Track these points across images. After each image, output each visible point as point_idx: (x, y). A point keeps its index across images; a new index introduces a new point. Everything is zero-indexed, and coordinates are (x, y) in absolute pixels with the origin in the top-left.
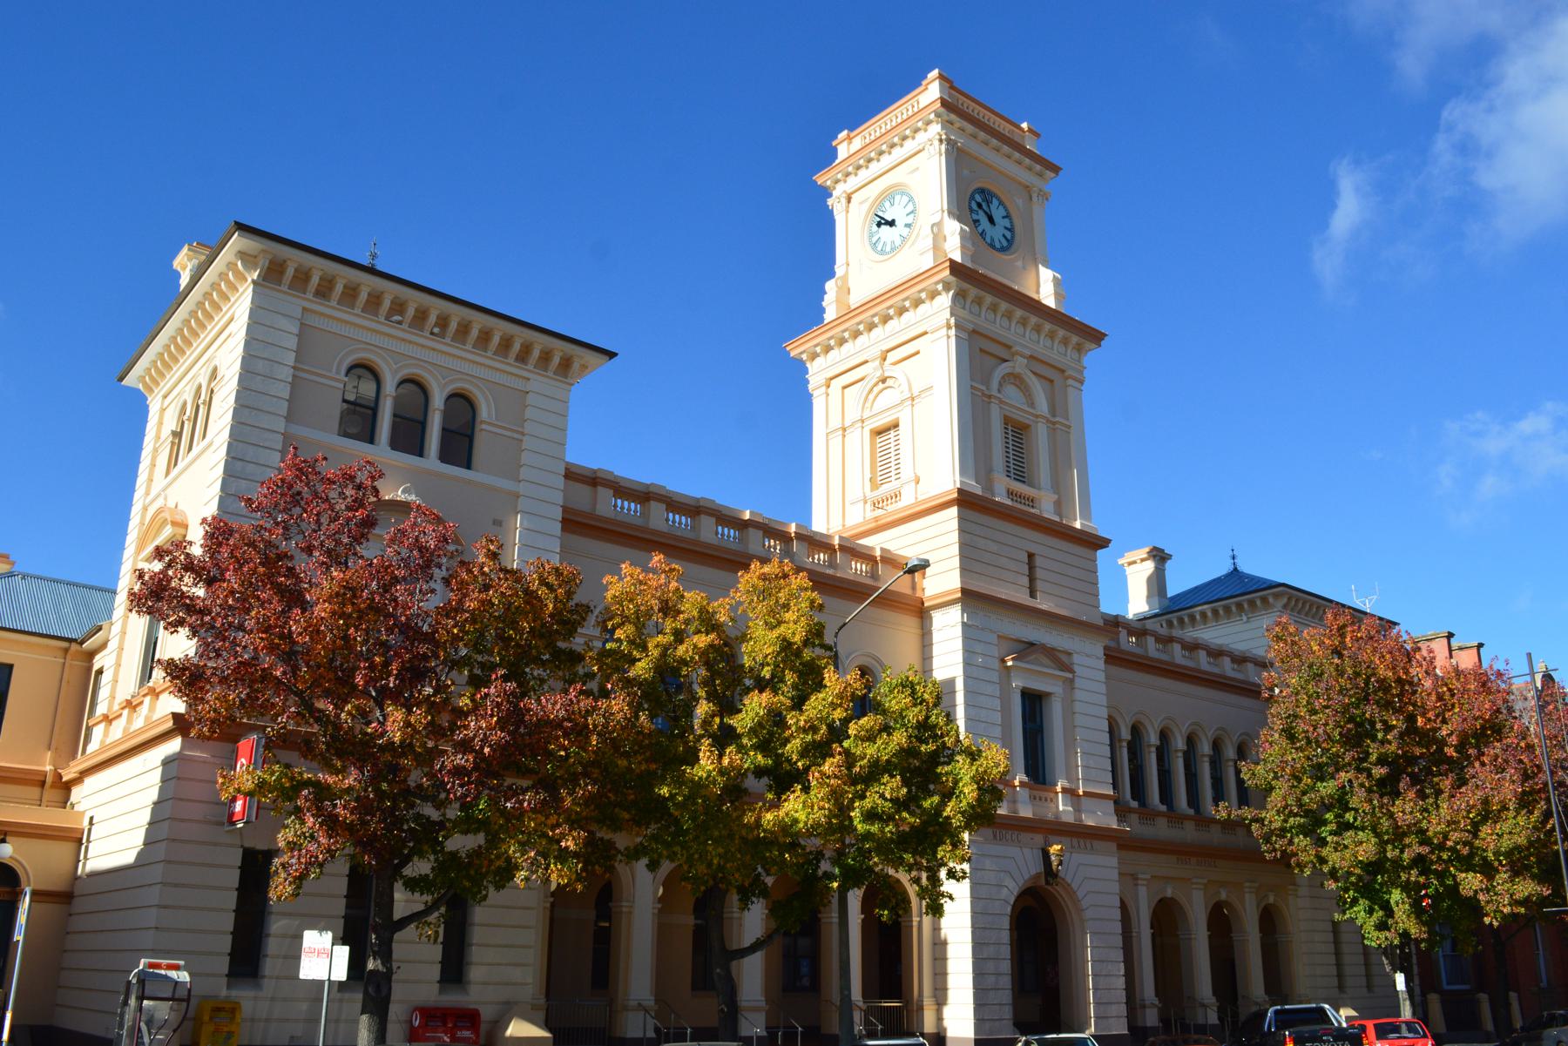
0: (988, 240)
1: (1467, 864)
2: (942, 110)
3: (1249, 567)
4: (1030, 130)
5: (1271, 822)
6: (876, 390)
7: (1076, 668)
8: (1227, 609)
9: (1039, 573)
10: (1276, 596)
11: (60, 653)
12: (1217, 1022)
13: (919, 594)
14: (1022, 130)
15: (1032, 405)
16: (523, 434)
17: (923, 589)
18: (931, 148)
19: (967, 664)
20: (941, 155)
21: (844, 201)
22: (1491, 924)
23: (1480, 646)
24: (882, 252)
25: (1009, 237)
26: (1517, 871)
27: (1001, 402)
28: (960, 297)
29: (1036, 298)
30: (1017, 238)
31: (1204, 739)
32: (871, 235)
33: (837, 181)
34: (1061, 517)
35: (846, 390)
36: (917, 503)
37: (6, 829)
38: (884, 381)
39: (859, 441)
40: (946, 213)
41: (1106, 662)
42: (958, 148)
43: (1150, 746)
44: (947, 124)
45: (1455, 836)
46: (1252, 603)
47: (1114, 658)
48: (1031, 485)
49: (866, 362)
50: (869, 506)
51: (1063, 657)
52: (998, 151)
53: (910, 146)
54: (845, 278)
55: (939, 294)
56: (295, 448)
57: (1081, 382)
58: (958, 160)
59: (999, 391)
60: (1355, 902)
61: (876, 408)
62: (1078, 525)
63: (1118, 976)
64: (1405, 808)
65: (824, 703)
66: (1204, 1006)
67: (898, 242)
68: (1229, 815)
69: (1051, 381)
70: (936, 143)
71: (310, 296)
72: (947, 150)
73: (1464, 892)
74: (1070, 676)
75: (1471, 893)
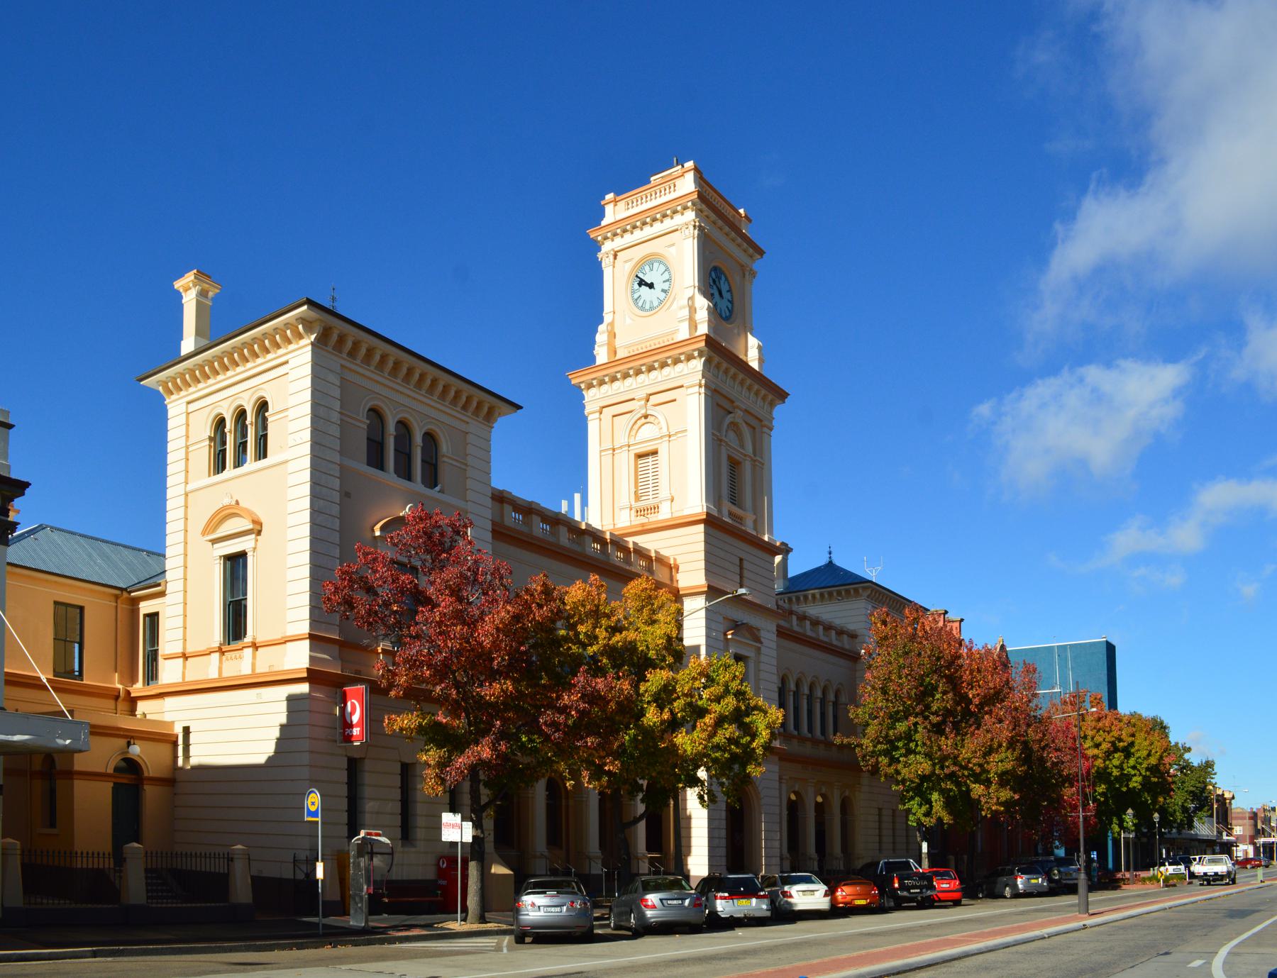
0: (718, 310)
1: (977, 778)
2: (698, 200)
3: (839, 562)
4: (746, 217)
5: (867, 747)
6: (640, 423)
7: (762, 640)
8: (830, 594)
9: (746, 573)
10: (864, 588)
11: (113, 599)
12: (817, 869)
13: (675, 585)
14: (740, 214)
15: (742, 446)
16: (466, 465)
17: (677, 581)
18: (687, 231)
19: (708, 636)
20: (694, 238)
21: (611, 257)
22: (986, 816)
23: (962, 620)
24: (642, 308)
25: (730, 308)
26: (1003, 783)
27: (727, 444)
28: (707, 364)
29: (745, 360)
30: (735, 309)
31: (790, 678)
32: (633, 292)
33: (606, 238)
34: (757, 532)
35: (614, 418)
36: (672, 519)
37: (133, 734)
38: (646, 417)
39: (625, 461)
40: (696, 289)
41: (777, 636)
42: (705, 234)
43: (790, 691)
44: (699, 212)
45: (975, 761)
46: (848, 591)
47: (782, 633)
48: (740, 507)
49: (633, 399)
50: (633, 512)
51: (755, 631)
52: (733, 240)
53: (668, 224)
54: (612, 324)
55: (694, 358)
56: (422, 504)
57: (771, 429)
58: (706, 245)
59: (726, 436)
60: (912, 798)
61: (638, 439)
62: (766, 538)
63: (776, 840)
64: (946, 744)
65: (689, 677)
66: (810, 859)
67: (656, 303)
68: (842, 742)
69: (754, 428)
70: (691, 228)
71: (344, 356)
72: (698, 235)
73: (973, 796)
74: (759, 645)
75: (977, 797)
